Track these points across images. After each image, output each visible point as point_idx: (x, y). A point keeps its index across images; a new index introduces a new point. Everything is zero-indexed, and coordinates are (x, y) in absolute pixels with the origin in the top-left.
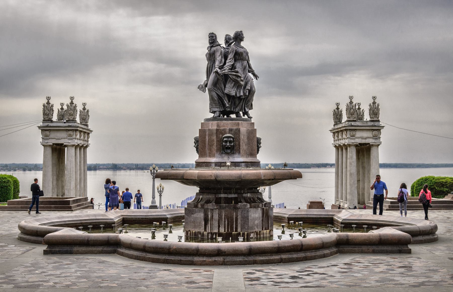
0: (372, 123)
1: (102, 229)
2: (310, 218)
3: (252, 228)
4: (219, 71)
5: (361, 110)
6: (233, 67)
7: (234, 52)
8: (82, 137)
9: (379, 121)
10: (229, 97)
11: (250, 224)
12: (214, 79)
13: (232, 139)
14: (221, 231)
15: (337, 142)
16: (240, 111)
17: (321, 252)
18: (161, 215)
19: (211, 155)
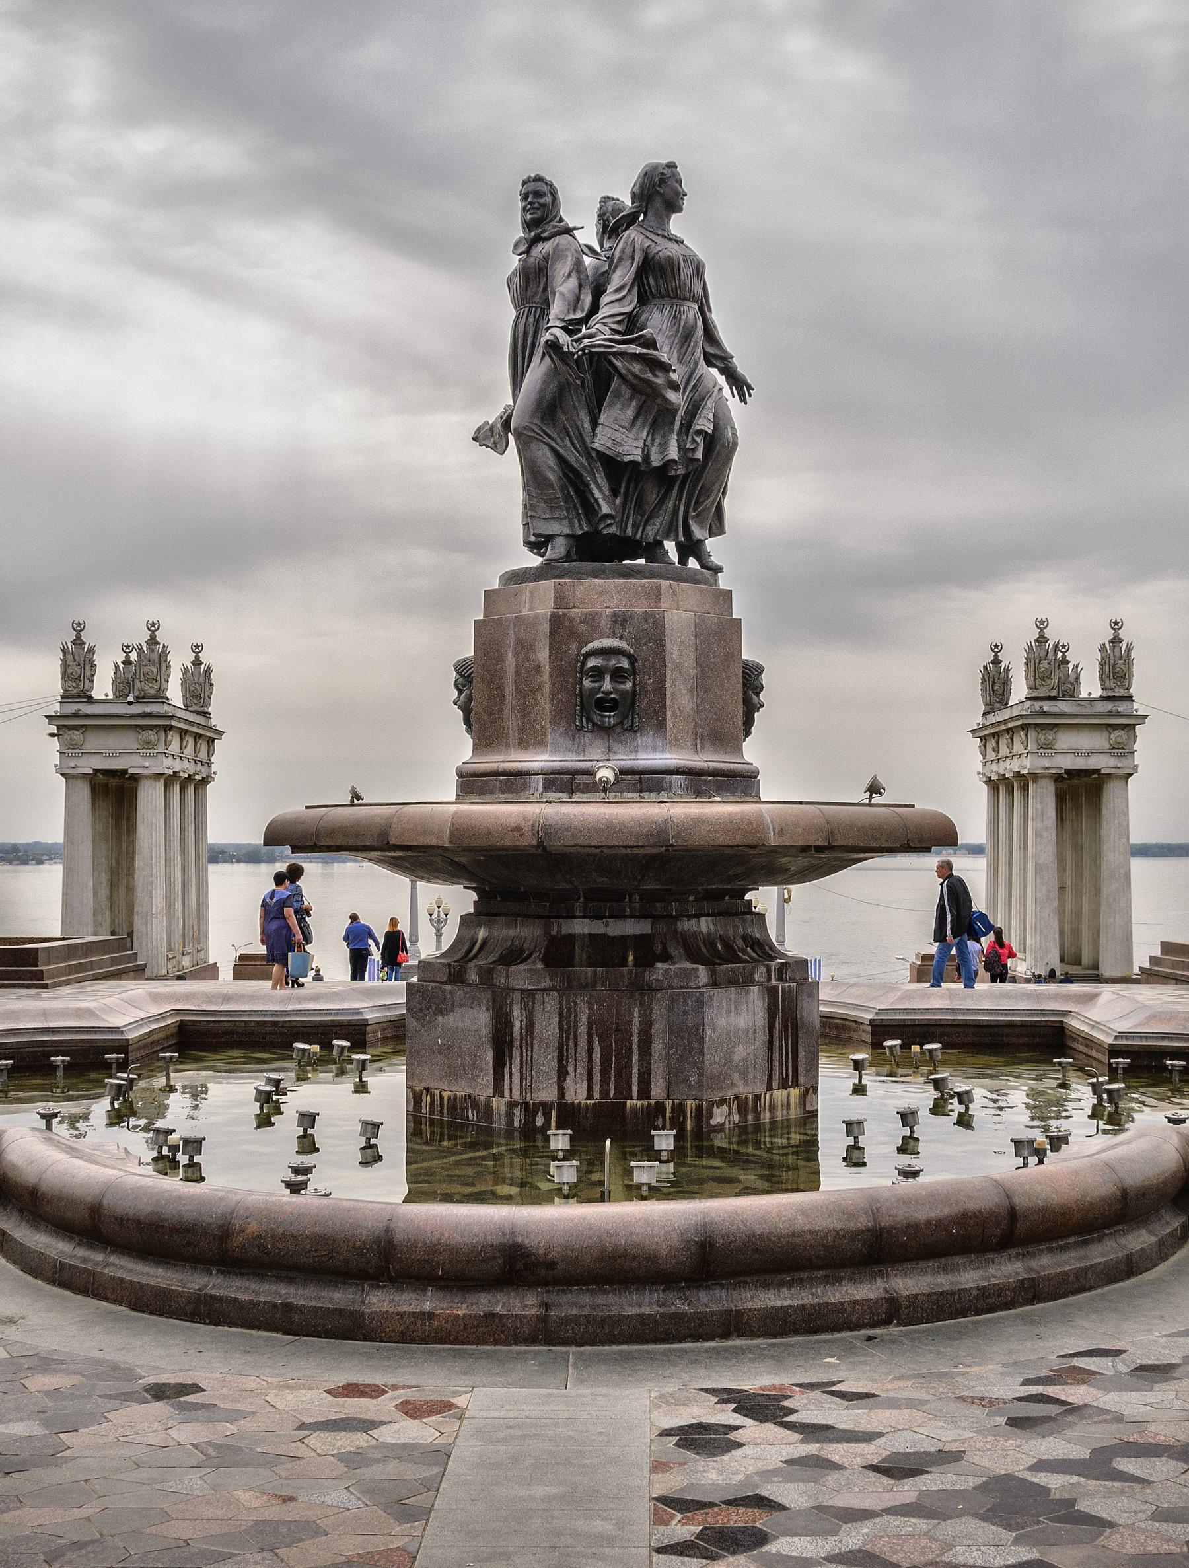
0: (1109, 706)
1: (60, 1073)
2: (966, 1025)
3: (719, 1081)
4: (564, 339)
5: (1071, 666)
6: (631, 322)
7: (638, 256)
8: (189, 751)
9: (1130, 699)
10: (612, 466)
11: (712, 1061)
12: (545, 383)
13: (625, 663)
14: (569, 1096)
15: (994, 767)
16: (667, 537)
17: (1109, 1244)
18: (339, 1012)
19: (529, 739)
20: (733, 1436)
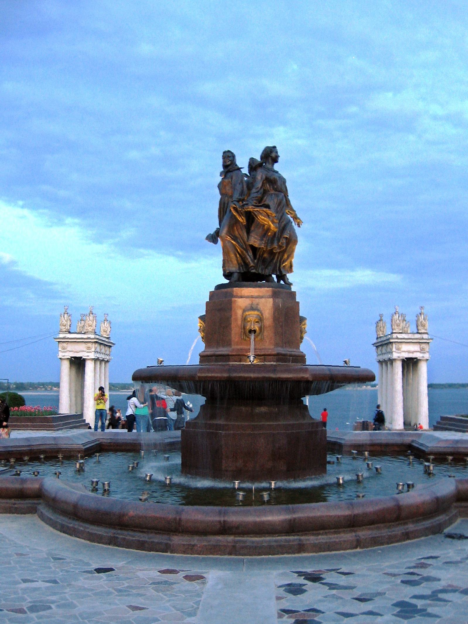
10: (254, 249)
20: (304, 587)
